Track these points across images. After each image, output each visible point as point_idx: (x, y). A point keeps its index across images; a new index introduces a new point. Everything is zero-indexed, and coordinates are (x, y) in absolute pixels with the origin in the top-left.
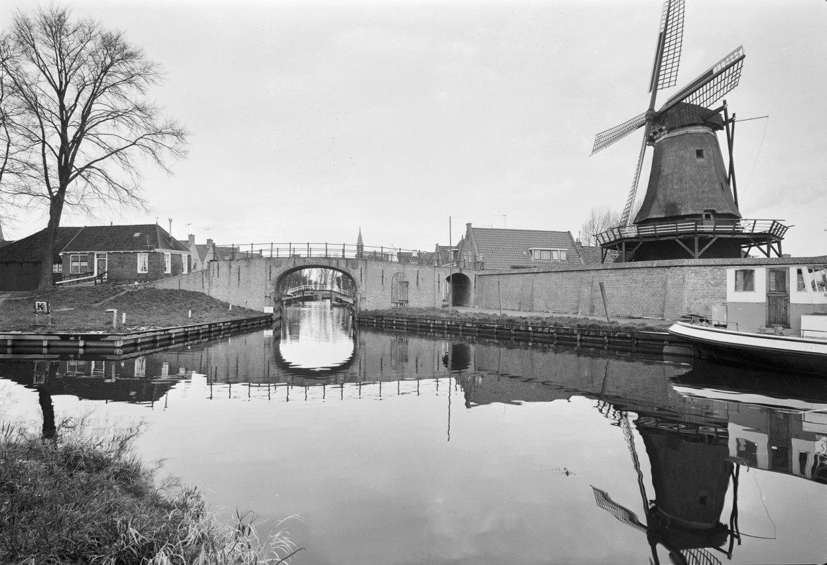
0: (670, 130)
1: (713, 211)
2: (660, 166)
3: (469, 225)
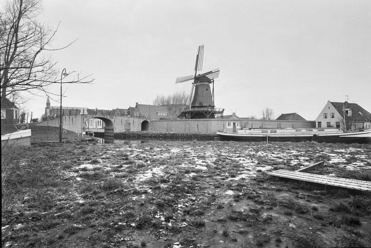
0: (200, 82)
1: (210, 105)
2: (198, 92)
3: (137, 103)
